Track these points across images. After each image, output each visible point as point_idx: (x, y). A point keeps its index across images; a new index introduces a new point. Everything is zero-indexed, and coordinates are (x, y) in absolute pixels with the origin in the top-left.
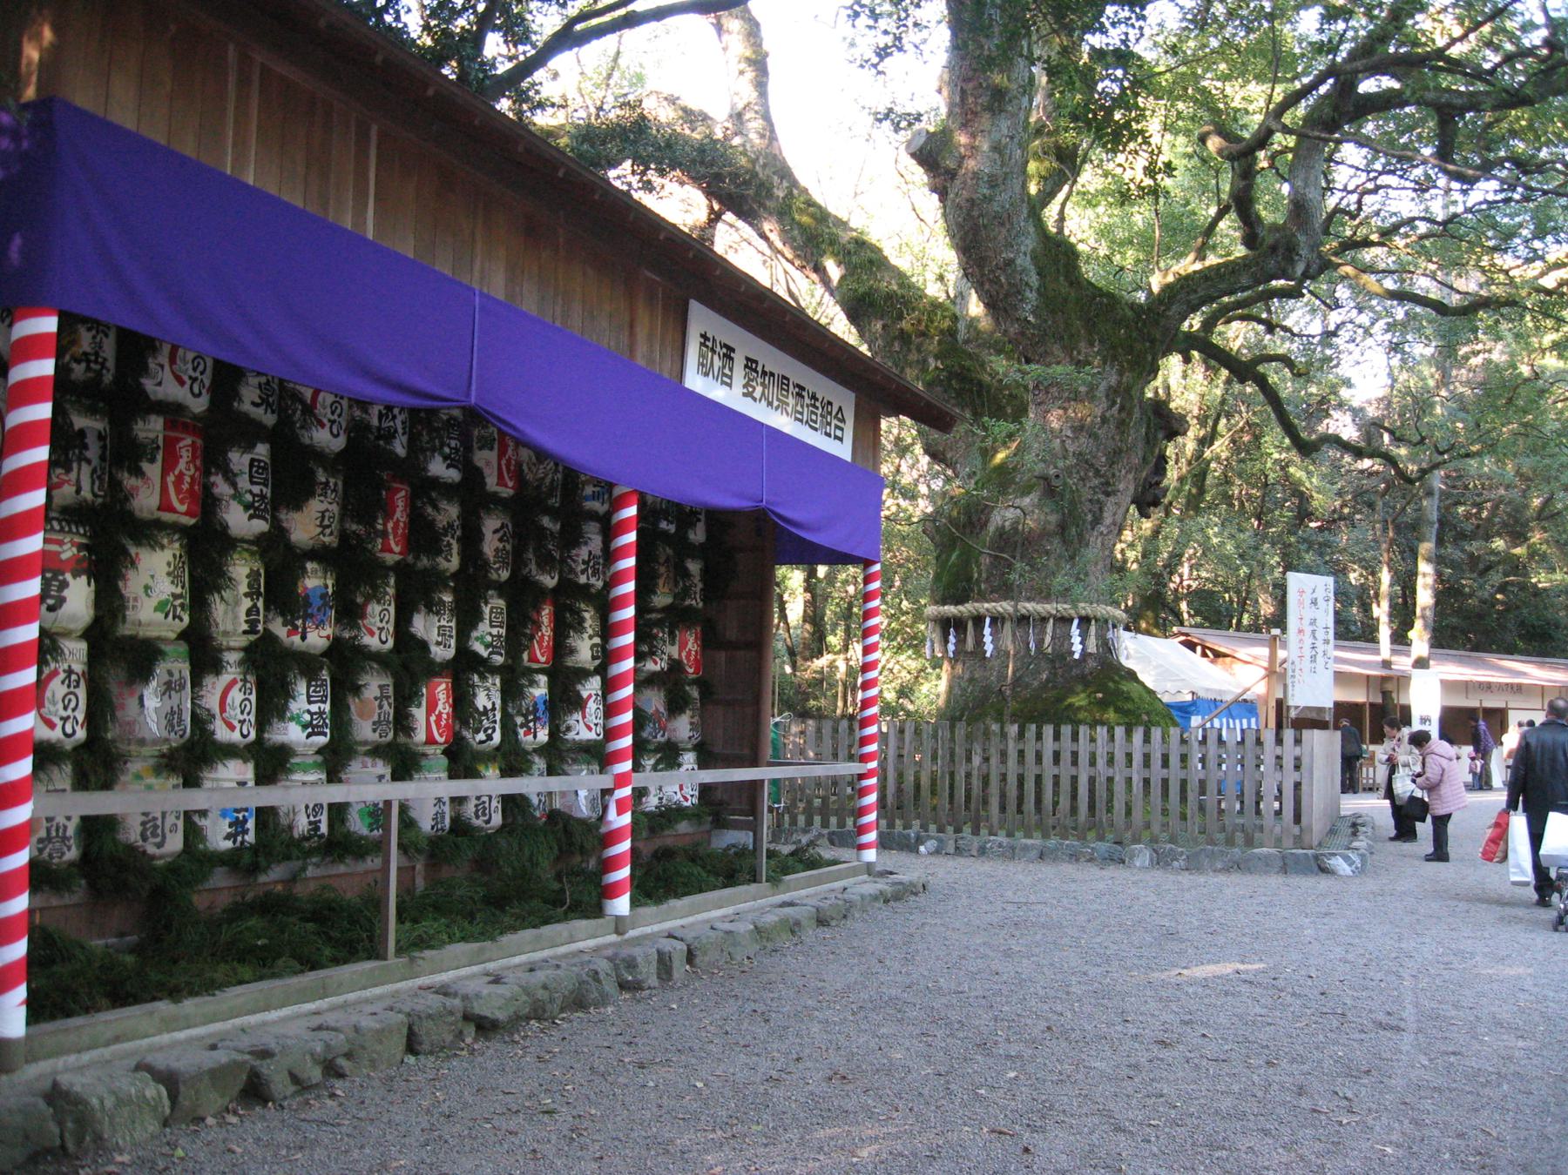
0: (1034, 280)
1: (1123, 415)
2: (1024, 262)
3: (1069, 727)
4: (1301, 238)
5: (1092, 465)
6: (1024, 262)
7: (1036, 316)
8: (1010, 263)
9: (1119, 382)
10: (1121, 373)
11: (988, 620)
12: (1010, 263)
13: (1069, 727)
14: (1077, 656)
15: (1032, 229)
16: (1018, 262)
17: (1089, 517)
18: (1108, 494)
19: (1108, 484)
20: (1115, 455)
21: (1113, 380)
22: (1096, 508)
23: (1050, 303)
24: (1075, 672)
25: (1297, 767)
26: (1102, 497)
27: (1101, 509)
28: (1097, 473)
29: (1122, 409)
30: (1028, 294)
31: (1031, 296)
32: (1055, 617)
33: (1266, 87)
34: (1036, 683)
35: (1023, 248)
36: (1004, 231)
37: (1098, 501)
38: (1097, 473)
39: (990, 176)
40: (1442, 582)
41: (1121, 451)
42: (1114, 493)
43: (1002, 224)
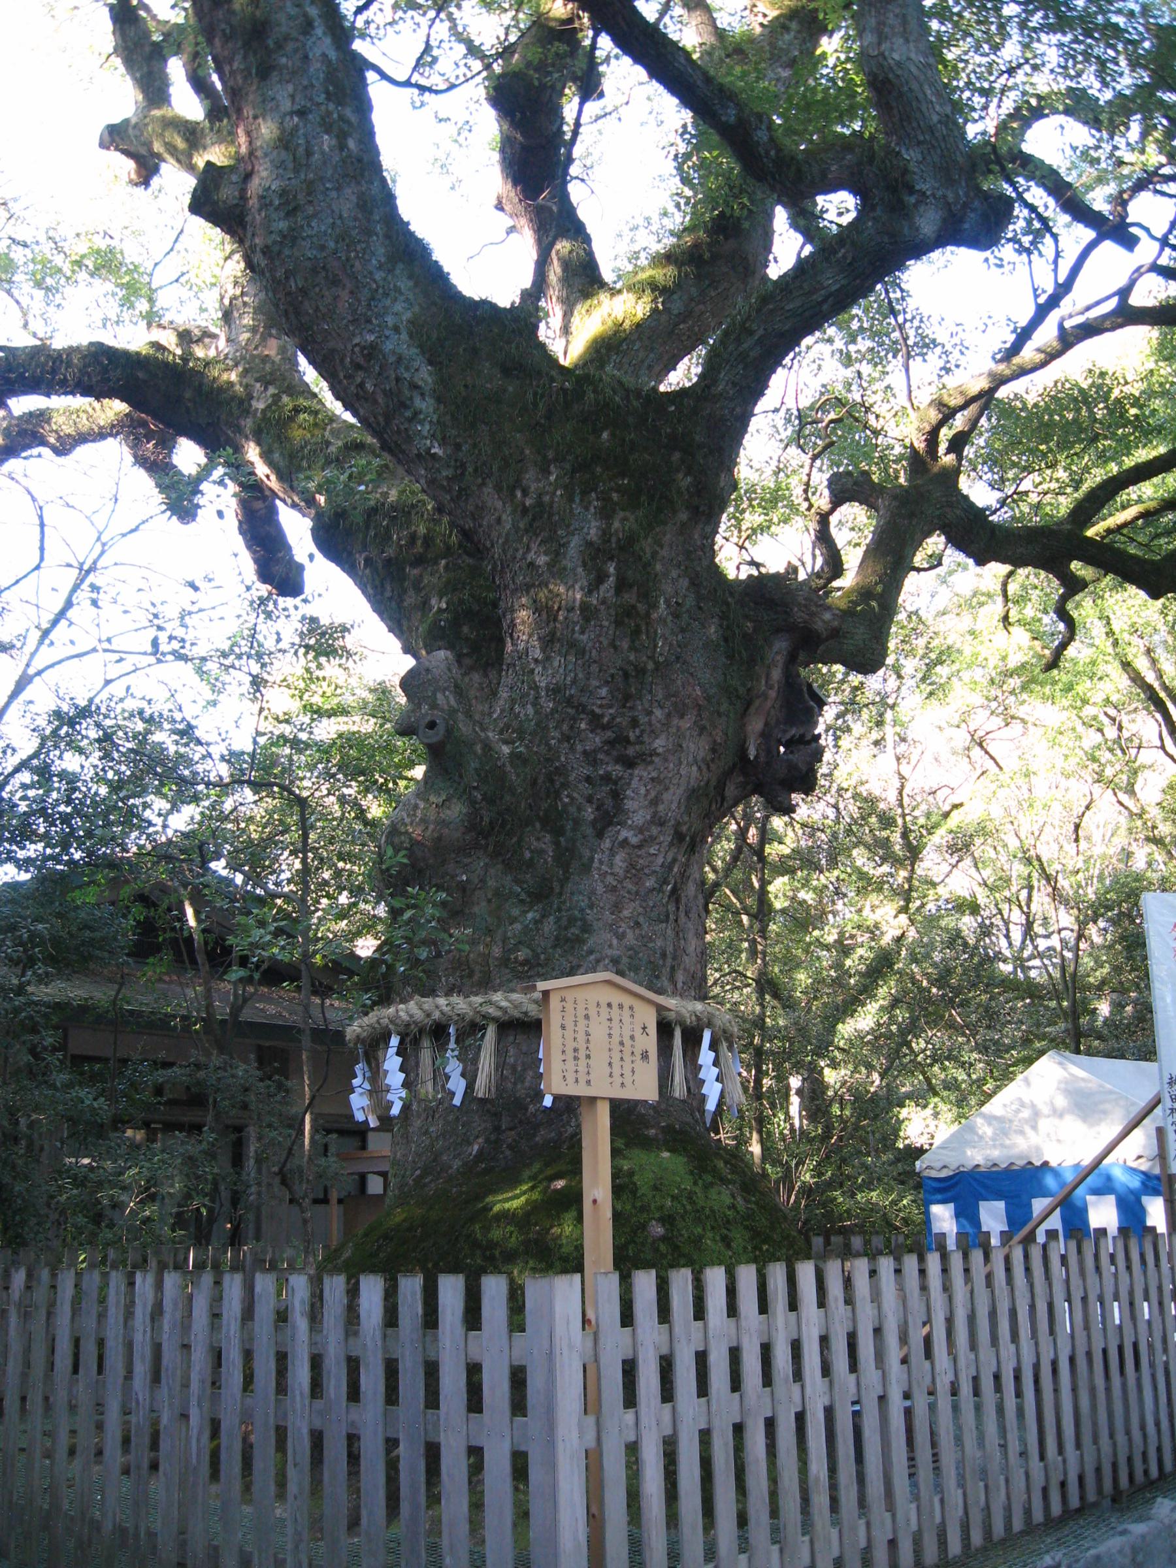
0: (425, 375)
1: (630, 597)
2: (398, 344)
3: (753, 1268)
4: (911, 155)
5: (581, 708)
6: (398, 344)
7: (443, 442)
8: (371, 352)
9: (605, 534)
10: (606, 514)
11: (395, 1041)
12: (371, 352)
13: (753, 1268)
14: (457, 1101)
15: (404, 284)
16: (388, 346)
17: (589, 813)
18: (629, 764)
19: (621, 740)
20: (629, 683)
21: (593, 530)
22: (603, 792)
23: (464, 411)
24: (543, 1135)
25: (519, 1406)
26: (616, 770)
27: (617, 796)
28: (596, 722)
29: (622, 585)
30: (419, 403)
31: (425, 405)
32: (495, 1020)
33: (1163, 160)
34: (456, 1164)
35: (390, 320)
36: (345, 295)
37: (607, 778)
38: (596, 722)
39: (283, 193)
40: (118, 433)
41: (641, 671)
42: (646, 757)
43: (335, 282)
